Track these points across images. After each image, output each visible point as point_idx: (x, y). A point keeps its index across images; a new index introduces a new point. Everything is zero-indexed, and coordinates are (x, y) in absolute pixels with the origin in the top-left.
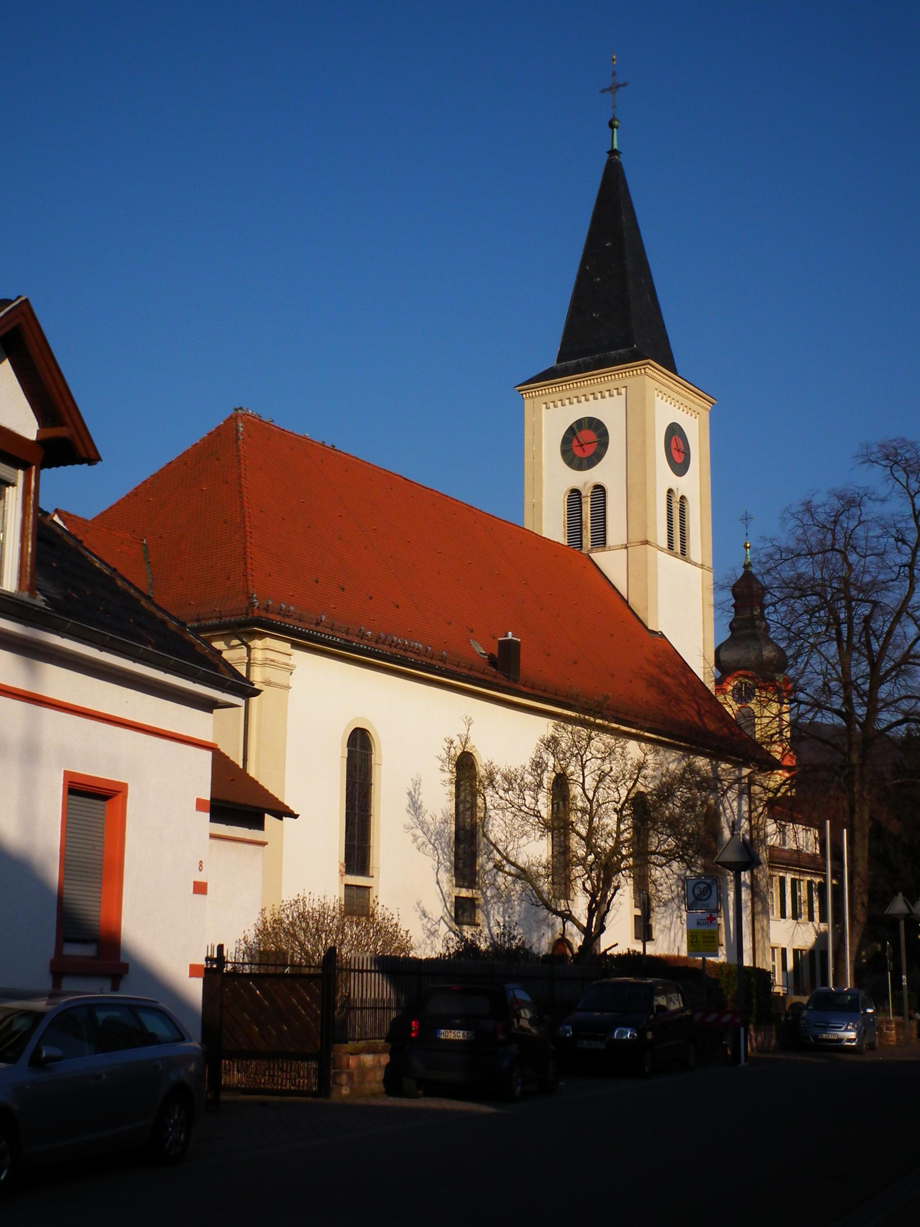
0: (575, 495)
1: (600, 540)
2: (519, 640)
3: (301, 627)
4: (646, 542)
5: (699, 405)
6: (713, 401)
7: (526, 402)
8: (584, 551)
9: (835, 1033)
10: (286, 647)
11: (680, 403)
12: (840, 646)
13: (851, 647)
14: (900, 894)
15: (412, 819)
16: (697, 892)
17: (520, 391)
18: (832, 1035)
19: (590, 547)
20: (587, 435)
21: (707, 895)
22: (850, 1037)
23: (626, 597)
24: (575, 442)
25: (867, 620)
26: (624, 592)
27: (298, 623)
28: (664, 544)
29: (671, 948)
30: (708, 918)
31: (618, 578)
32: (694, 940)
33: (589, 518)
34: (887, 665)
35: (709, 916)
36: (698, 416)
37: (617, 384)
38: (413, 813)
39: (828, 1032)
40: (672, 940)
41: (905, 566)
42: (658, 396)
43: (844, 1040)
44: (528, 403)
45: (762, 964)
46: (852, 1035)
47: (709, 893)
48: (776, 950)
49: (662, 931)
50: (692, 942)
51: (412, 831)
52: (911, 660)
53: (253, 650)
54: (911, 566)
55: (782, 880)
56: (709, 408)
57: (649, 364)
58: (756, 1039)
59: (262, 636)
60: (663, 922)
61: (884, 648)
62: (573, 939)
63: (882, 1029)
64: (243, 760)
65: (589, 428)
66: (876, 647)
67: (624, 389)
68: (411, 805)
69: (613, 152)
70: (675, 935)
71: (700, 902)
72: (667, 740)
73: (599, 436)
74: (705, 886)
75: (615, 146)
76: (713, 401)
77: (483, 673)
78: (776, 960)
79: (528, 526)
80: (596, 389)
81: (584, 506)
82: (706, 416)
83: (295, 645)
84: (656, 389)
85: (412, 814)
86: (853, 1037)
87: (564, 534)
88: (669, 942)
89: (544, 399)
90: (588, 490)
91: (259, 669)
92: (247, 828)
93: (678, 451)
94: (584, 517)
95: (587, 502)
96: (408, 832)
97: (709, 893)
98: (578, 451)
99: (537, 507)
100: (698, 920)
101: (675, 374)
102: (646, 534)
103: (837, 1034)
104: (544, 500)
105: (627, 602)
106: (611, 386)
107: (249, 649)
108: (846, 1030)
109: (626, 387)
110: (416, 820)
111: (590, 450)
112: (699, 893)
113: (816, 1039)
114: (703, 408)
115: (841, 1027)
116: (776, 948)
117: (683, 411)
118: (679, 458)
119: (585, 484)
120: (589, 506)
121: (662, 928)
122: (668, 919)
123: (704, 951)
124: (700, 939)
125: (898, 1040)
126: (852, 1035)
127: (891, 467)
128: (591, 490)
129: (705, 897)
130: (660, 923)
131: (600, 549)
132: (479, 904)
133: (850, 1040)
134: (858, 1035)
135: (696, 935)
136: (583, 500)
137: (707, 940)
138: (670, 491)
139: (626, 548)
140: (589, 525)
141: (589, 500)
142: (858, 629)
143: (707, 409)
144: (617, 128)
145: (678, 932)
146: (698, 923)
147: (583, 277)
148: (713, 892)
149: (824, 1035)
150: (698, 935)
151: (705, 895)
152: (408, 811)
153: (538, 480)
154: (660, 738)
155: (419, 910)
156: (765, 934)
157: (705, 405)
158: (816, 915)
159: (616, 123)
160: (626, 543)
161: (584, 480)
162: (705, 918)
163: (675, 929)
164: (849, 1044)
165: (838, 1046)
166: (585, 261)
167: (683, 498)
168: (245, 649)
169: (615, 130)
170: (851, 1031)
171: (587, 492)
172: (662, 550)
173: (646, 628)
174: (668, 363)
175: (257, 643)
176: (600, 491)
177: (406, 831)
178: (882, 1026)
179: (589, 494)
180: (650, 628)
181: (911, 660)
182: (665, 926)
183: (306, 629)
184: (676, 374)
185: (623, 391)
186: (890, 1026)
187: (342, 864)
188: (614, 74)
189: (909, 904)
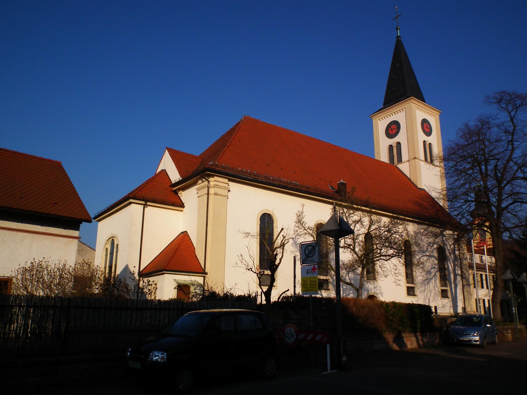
0: (391, 147)
1: (400, 161)
2: (345, 182)
3: (231, 172)
4: (415, 158)
5: (434, 113)
6: (440, 111)
7: (373, 120)
8: (395, 165)
9: (468, 337)
10: (226, 181)
11: (426, 112)
13: (487, 175)
14: (509, 270)
15: (294, 249)
16: (307, 252)
17: (371, 117)
18: (466, 339)
19: (397, 163)
20: (394, 126)
21: (313, 254)
22: (477, 339)
23: (410, 178)
24: (390, 129)
26: (409, 177)
27: (223, 169)
28: (423, 159)
29: (425, 298)
30: (312, 269)
31: (407, 172)
32: (305, 283)
33: (396, 154)
35: (313, 267)
36: (434, 117)
37: (402, 107)
38: (295, 246)
39: (463, 337)
40: (425, 295)
42: (417, 110)
43: (473, 341)
44: (374, 121)
45: (216, 288)
46: (477, 338)
47: (314, 252)
48: (480, 300)
49: (420, 292)
50: (304, 285)
51: (294, 253)
53: (210, 182)
55: (481, 275)
56: (439, 114)
57: (412, 98)
58: (422, 340)
59: (213, 176)
60: (421, 289)
61: (502, 174)
62: (378, 295)
63: (503, 333)
64: (206, 224)
65: (394, 124)
66: (499, 175)
67: (404, 109)
68: (294, 243)
69: (398, 37)
70: (427, 294)
71: (309, 258)
72: (418, 220)
73: (397, 126)
74: (312, 247)
75: (399, 35)
76: (440, 111)
77: (328, 194)
78: (481, 303)
79: (376, 158)
80: (395, 111)
81: (394, 150)
82: (438, 117)
83: (230, 180)
84: (416, 107)
85: (294, 247)
86: (478, 339)
87: (388, 160)
88: (424, 296)
89: (379, 118)
90: (395, 144)
91: (213, 189)
92: (62, 228)
93: (427, 128)
94: (394, 154)
95: (395, 148)
96: (292, 254)
97: (314, 252)
98: (391, 132)
99: (379, 153)
100: (307, 270)
101: (424, 102)
102: (415, 156)
103: (468, 338)
104: (381, 150)
105: (410, 179)
106: (400, 109)
107: (209, 182)
108: (473, 336)
109: (405, 108)
110: (296, 249)
111: (395, 131)
112: (308, 252)
113: (457, 340)
114: (437, 114)
115: (471, 334)
116: (481, 299)
117: (428, 115)
118: (428, 130)
119: (394, 143)
120: (396, 150)
121: (421, 291)
122: (423, 288)
123: (310, 291)
124: (308, 282)
125: (513, 338)
126: (477, 338)
128: (396, 144)
129: (311, 255)
130: (419, 289)
131: (400, 163)
132: (330, 282)
133: (476, 341)
134: (480, 338)
135: (306, 280)
136: (393, 148)
137: (313, 283)
138: (424, 142)
139: (409, 161)
140: (396, 156)
141: (395, 148)
143: (438, 114)
144: (399, 29)
145: (428, 293)
146: (307, 273)
147: (390, 77)
148: (316, 251)
149: (461, 338)
150: (307, 280)
151: (312, 254)
152: (292, 246)
153: (378, 144)
154: (415, 220)
155: (299, 284)
156: (469, 293)
157: (438, 114)
158: (485, 286)
159: (398, 27)
160: (408, 159)
161: (393, 141)
162: (311, 269)
163: (427, 291)
164: (475, 343)
165: (470, 344)
166: (391, 72)
167: (430, 144)
168: (207, 182)
169: (398, 30)
170: (476, 336)
171: (394, 145)
172: (422, 161)
173: (417, 187)
174: (421, 97)
175: (211, 179)
176: (399, 144)
177: (291, 253)
178: (504, 332)
179: (395, 146)
180: (419, 187)
182: (422, 290)
184: (425, 103)
185: (404, 109)
186: (507, 332)
187: (258, 266)
189: (513, 274)
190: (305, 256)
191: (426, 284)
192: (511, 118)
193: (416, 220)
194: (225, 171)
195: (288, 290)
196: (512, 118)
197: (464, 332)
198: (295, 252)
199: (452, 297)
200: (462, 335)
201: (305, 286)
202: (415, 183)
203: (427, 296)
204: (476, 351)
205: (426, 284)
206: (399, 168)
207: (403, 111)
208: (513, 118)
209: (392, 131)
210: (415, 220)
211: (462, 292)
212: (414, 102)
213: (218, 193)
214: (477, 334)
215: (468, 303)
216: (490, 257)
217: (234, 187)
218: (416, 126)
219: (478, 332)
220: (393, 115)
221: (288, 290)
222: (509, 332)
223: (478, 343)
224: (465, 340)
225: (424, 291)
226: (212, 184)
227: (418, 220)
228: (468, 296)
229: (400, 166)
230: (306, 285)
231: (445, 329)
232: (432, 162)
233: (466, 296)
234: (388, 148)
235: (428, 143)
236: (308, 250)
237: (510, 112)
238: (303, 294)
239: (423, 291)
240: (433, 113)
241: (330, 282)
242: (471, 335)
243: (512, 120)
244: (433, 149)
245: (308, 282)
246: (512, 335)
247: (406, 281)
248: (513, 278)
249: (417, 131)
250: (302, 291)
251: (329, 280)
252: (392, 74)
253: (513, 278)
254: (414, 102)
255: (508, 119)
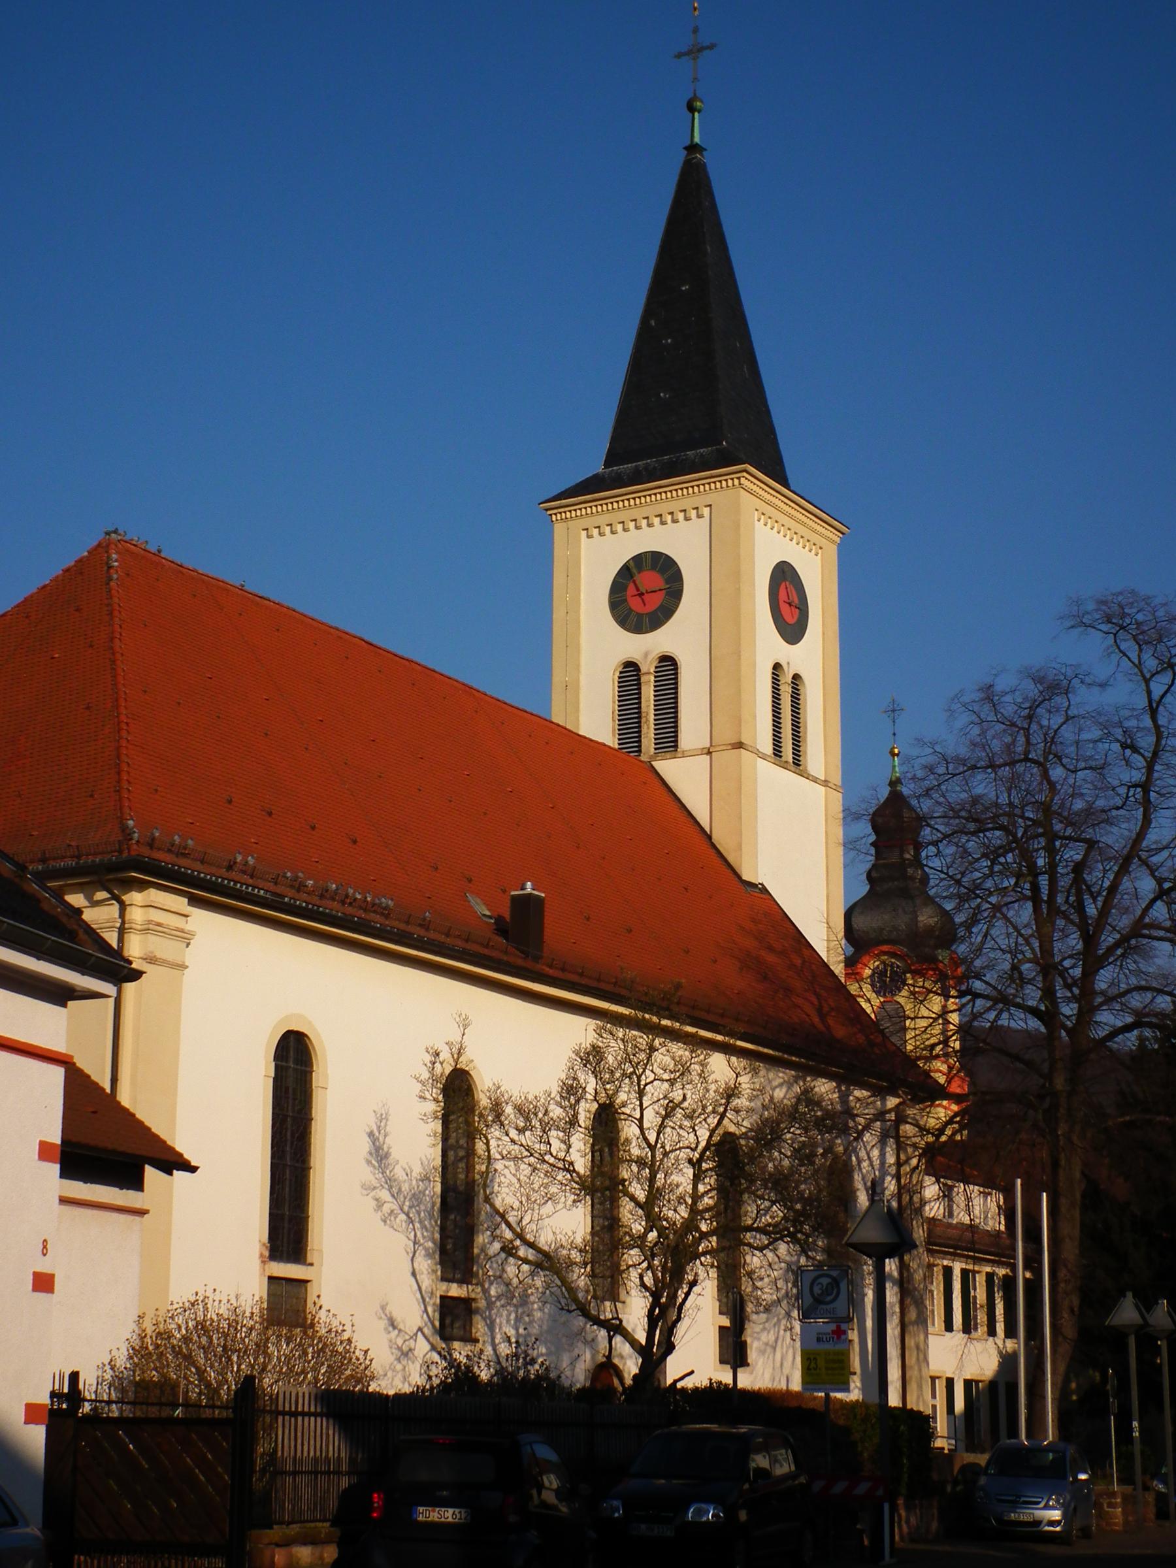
0: (630, 671)
1: (669, 741)
2: (543, 895)
4: (740, 745)
5: (821, 535)
7: (556, 526)
8: (643, 758)
10: (180, 903)
11: (793, 531)
12: (1036, 909)
13: (1054, 911)
14: (1130, 1295)
15: (374, 1174)
16: (817, 1290)
17: (547, 510)
19: (652, 751)
20: (650, 580)
22: (1053, 1519)
23: (708, 830)
24: (631, 589)
25: (1079, 868)
26: (704, 822)
28: (768, 749)
30: (834, 1332)
31: (697, 800)
32: (813, 1365)
34: (1108, 939)
38: (376, 1164)
40: (778, 1364)
41: (1136, 786)
44: (559, 529)
46: (1056, 1515)
47: (835, 1292)
48: (937, 1381)
49: (762, 1352)
50: (809, 1369)
51: (373, 1193)
52: (1146, 932)
53: (128, 909)
54: (1145, 786)
56: (838, 540)
57: (745, 471)
58: (908, 1522)
59: (142, 886)
62: (625, 1364)
63: (1101, 1505)
65: (653, 568)
68: (373, 1151)
71: (824, 1307)
72: (771, 1052)
75: (697, 139)
79: (558, 718)
82: (832, 551)
83: (195, 901)
85: (374, 1167)
87: (614, 730)
89: (585, 522)
90: (651, 663)
93: (790, 605)
94: (644, 709)
97: (835, 1292)
98: (635, 604)
99: (572, 688)
102: (740, 733)
105: (710, 837)
106: (687, 503)
107: (123, 907)
108: (1047, 1507)
109: (710, 506)
110: (381, 1175)
111: (655, 602)
112: (820, 1292)
113: (1000, 1520)
114: (829, 539)
115: (1038, 1503)
116: (938, 1378)
118: (791, 617)
119: (646, 655)
122: (772, 1332)
124: (821, 1363)
125: (1126, 1522)
126: (1056, 1515)
127: (1115, 635)
128: (655, 663)
130: (759, 1339)
131: (668, 755)
133: (1052, 1523)
134: (1064, 1515)
138: (777, 667)
139: (709, 753)
140: (652, 717)
141: (652, 678)
142: (1064, 882)
143: (833, 542)
145: (787, 1352)
146: (819, 1340)
151: (829, 1295)
152: (369, 1162)
153: (573, 645)
154: (761, 1049)
155: (383, 1316)
156: (921, 1356)
158: (1000, 1327)
159: (699, 104)
164: (1051, 1529)
169: (696, 114)
171: (648, 667)
172: (763, 757)
173: (739, 877)
175: (135, 897)
176: (668, 664)
177: (365, 1192)
179: (652, 670)
180: (745, 877)
181: (1146, 932)
182: (767, 1344)
183: (212, 875)
184: (787, 486)
187: (264, 1244)
188: (696, 30)
190: (812, 1300)
191: (781, 1317)
192: (1150, 701)
193: (766, 1050)
194: (187, 865)
195: (692, 1372)
196: (1154, 705)
197: (1020, 1497)
198: (375, 1188)
199: (862, 1370)
200: (1016, 1504)
201: (813, 1371)
202: (731, 859)
203: (782, 1364)
204: (1052, 1549)
205: (781, 1317)
206: (657, 768)
207: (699, 516)
208: (1159, 702)
209: (643, 590)
210: (761, 1049)
211: (899, 1352)
212: (751, 486)
213: (159, 954)
214: (1057, 1501)
215: (918, 1398)
216: (982, 1189)
217: (204, 922)
218: (753, 597)
219: (1059, 1495)
220: (650, 525)
221: (692, 1372)
222: (1119, 1500)
223: (1058, 1529)
224: (1021, 1519)
225: (774, 1348)
226: (136, 915)
227: (771, 1052)
228: (916, 1368)
229: (667, 768)
230: (815, 1369)
231: (949, 1489)
232: (797, 763)
233: (911, 1367)
234: (618, 674)
235: (791, 675)
236: (820, 1286)
237: (1148, 676)
238: (808, 1389)
239: (772, 1346)
240: (815, 538)
241: (477, 1311)
242: (1042, 1505)
243: (1153, 712)
244: (809, 710)
245: (821, 1363)
246: (1124, 1512)
247: (717, 1304)
248: (1140, 1321)
249: (753, 621)
250: (805, 1382)
251: (474, 1300)
252: (653, 322)
253: (1140, 1321)
254: (751, 486)
255: (1143, 702)
